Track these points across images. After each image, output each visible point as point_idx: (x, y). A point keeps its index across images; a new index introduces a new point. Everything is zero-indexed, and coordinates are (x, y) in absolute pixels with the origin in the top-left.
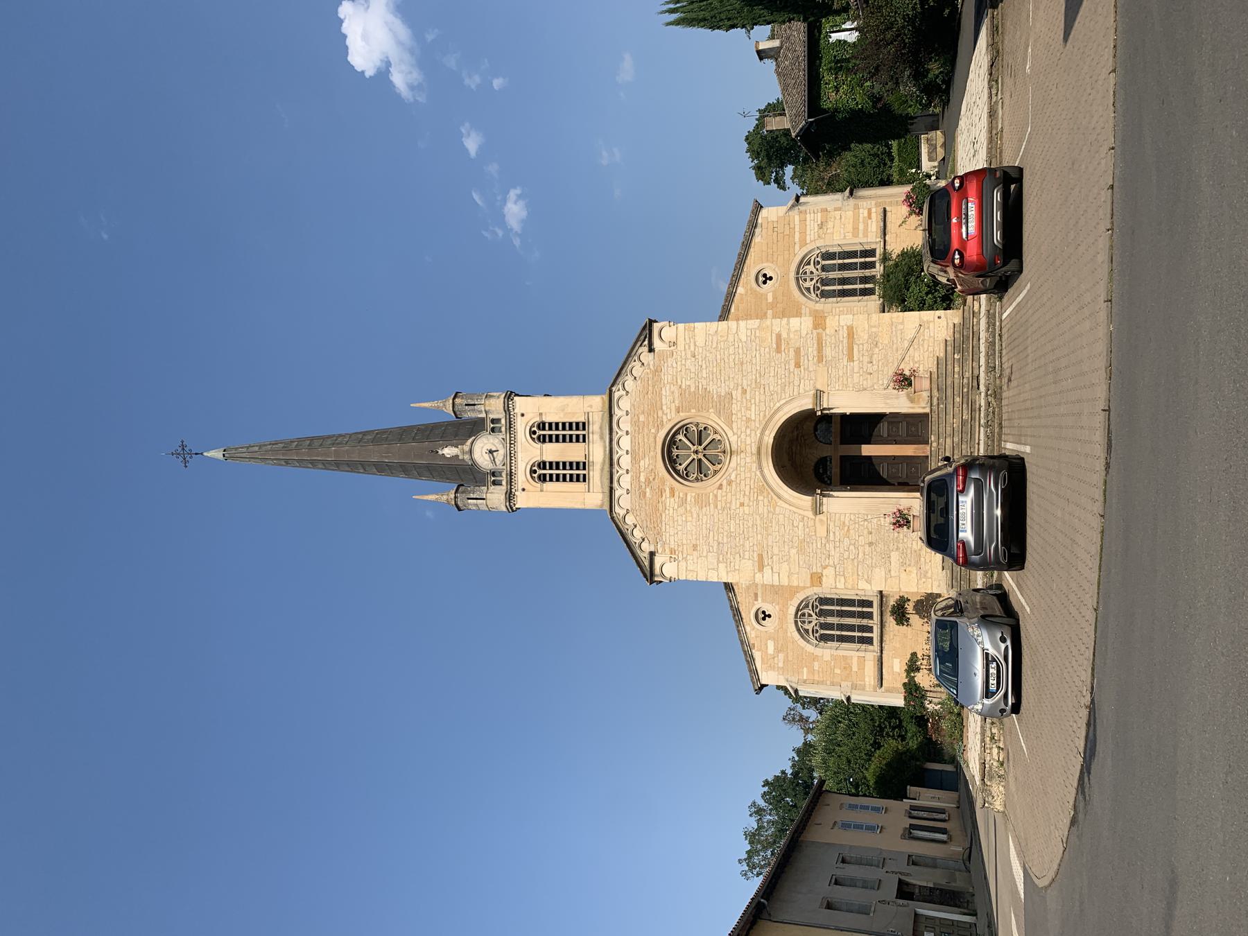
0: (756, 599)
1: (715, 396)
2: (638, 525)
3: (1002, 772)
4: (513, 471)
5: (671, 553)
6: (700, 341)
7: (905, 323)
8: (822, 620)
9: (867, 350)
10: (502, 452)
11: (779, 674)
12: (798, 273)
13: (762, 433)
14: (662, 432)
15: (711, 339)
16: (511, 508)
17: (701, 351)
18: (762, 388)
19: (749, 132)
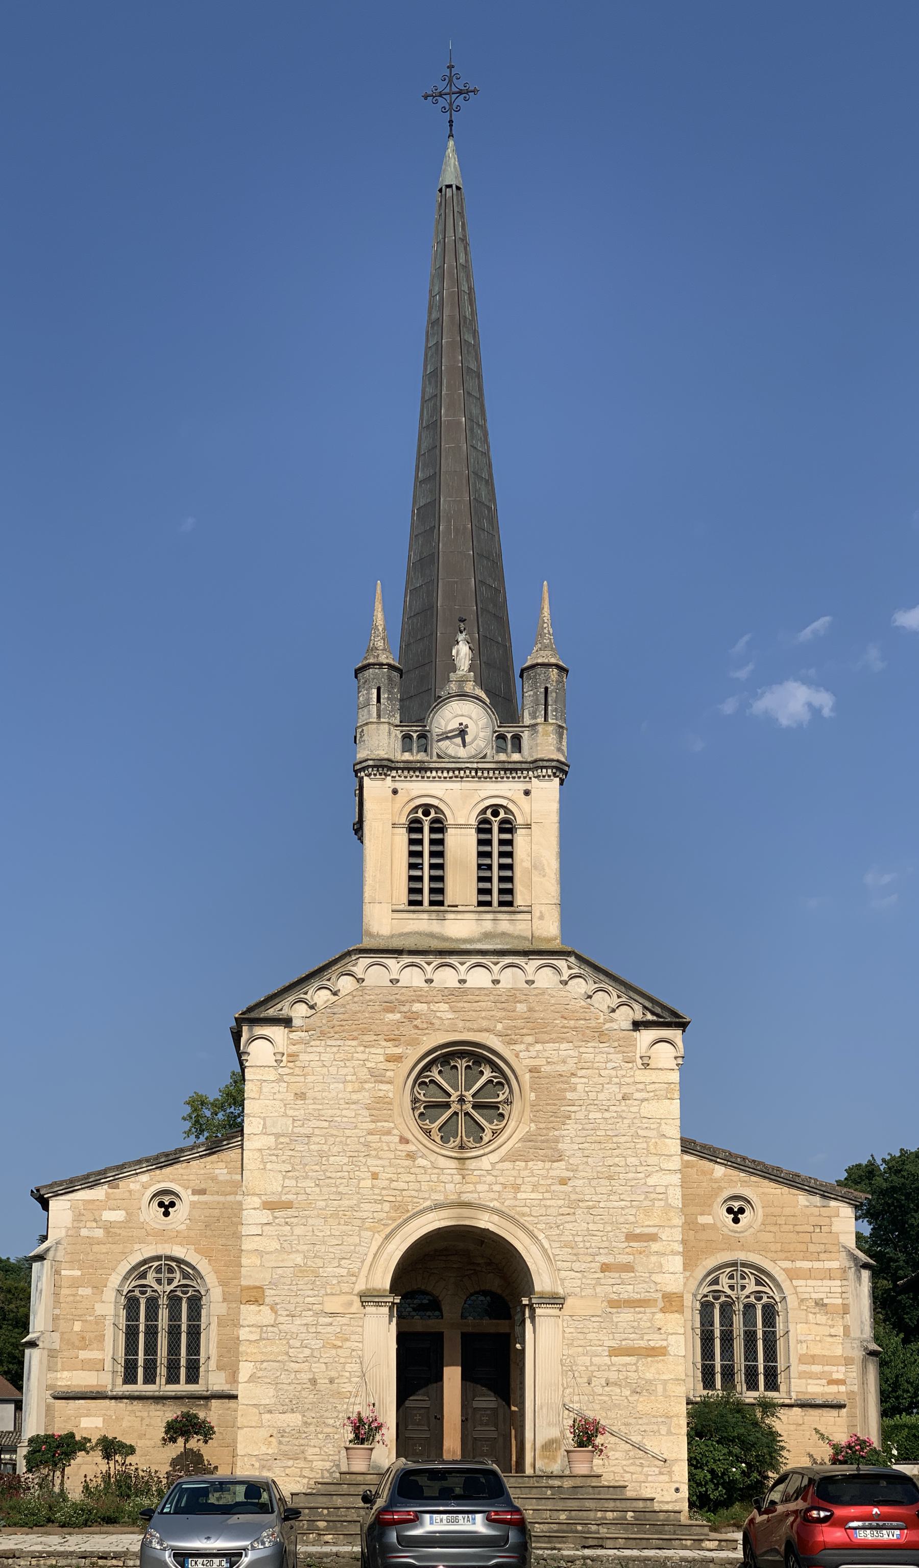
0: (195, 1192)
1: (556, 1133)
2: (337, 998)
4: (428, 774)
5: (289, 1055)
8: (163, 1301)
9: (627, 1378)
10: (462, 753)
11: (69, 1229)
12: (744, 1265)
13: (495, 1211)
15: (652, 1126)
16: (363, 769)
17: (633, 1109)
18: (568, 1210)
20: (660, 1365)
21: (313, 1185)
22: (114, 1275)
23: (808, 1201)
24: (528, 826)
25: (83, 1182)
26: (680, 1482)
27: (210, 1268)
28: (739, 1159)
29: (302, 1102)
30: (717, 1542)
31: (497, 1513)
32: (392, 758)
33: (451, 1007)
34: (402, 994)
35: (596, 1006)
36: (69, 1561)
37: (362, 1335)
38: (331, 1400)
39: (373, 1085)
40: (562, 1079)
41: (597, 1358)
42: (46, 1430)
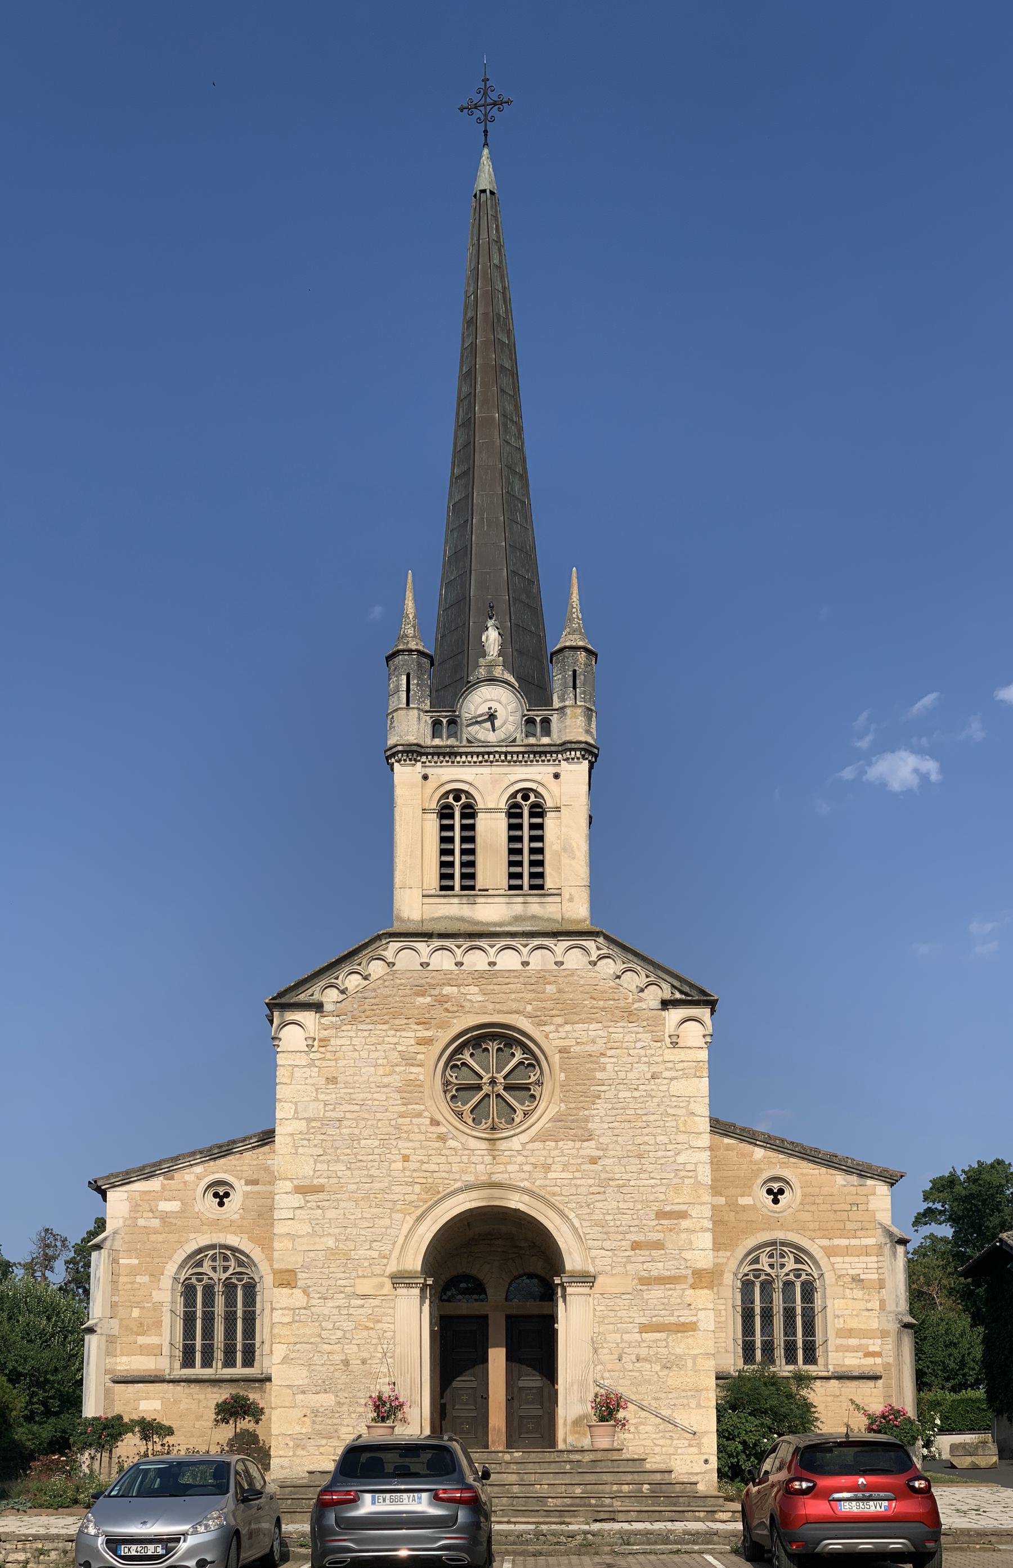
0: (247, 1183)
1: (586, 1113)
2: (367, 982)
4: (458, 759)
5: (321, 1040)
6: (678, 1087)
7: (701, 1411)
8: (219, 1288)
9: (657, 1354)
10: (492, 737)
11: (126, 1219)
12: (783, 1244)
14: (527, 1024)
15: (681, 1104)
18: (599, 1189)
20: (690, 1340)
21: (344, 1168)
22: (170, 1263)
23: (845, 1180)
24: (557, 809)
25: (139, 1173)
26: (710, 1454)
27: (263, 1256)
28: (778, 1142)
29: (334, 1086)
30: (731, 1513)
31: (445, 1491)
32: (422, 743)
33: (481, 990)
34: (432, 977)
35: (625, 986)
36: (55, 1545)
37: (394, 1316)
38: (363, 1380)
39: (404, 1068)
40: (591, 1059)
41: (627, 1335)
42: (105, 1413)
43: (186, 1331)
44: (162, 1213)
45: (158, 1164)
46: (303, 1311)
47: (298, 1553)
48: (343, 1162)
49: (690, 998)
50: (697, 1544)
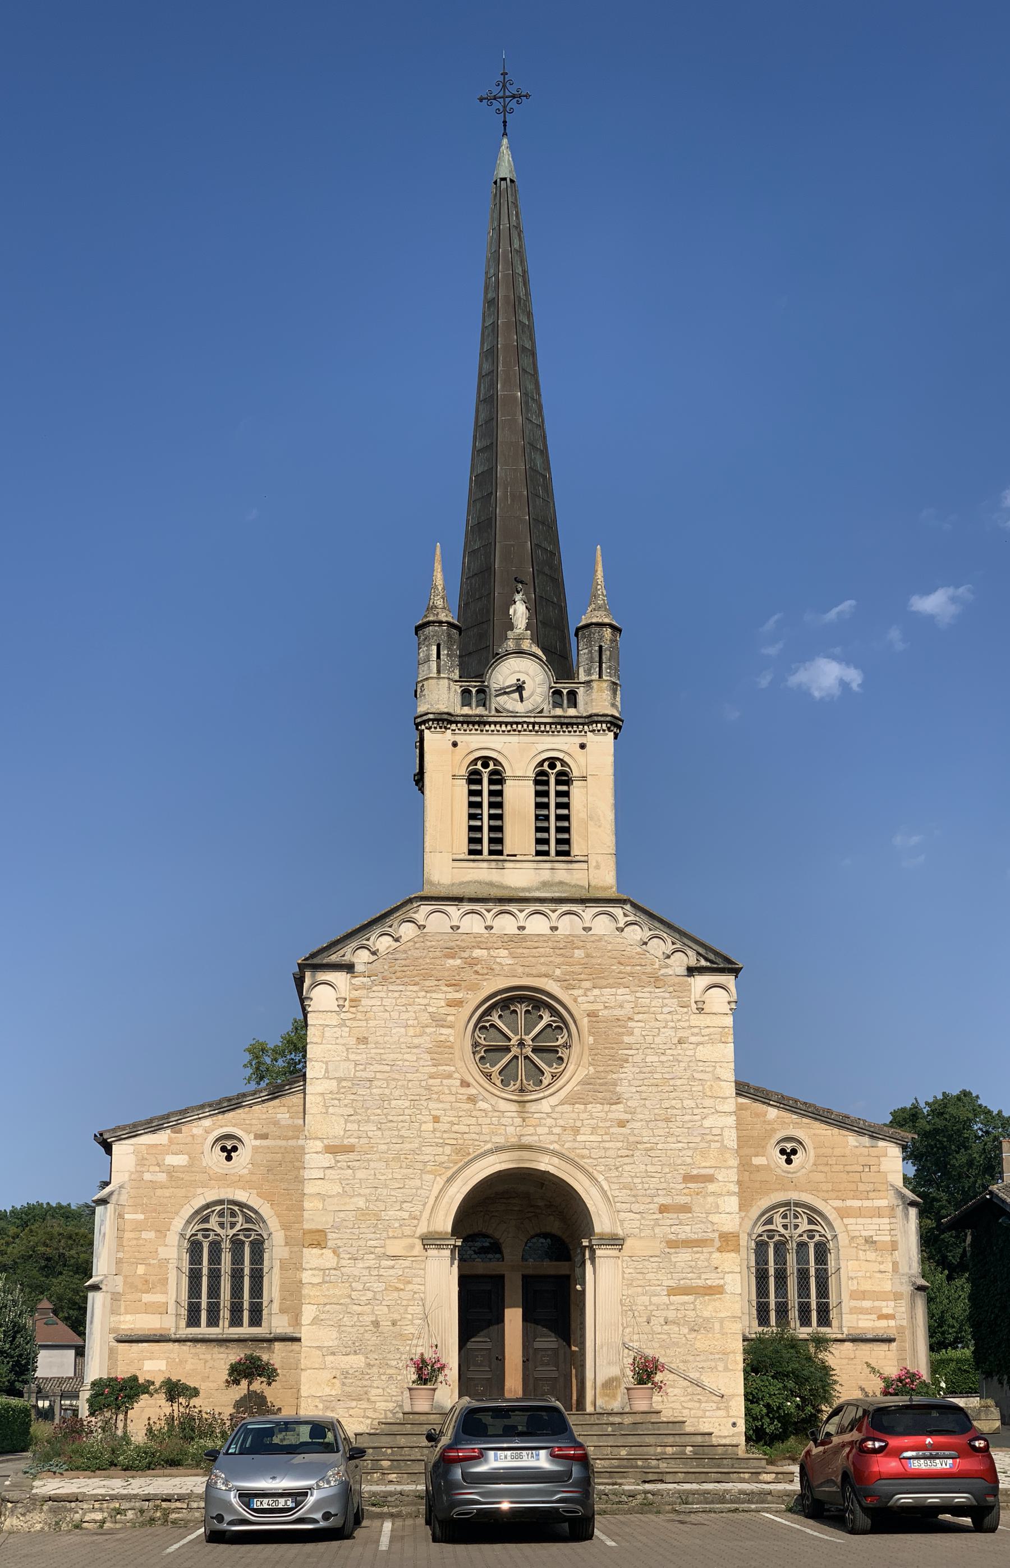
0: (257, 1137)
1: (614, 1076)
2: (398, 944)
3: (64, 1526)
4: (487, 727)
5: (351, 1000)
6: (703, 1052)
7: (728, 1374)
8: (226, 1245)
10: (520, 708)
11: (132, 1173)
12: (796, 1205)
13: (554, 1153)
14: (556, 988)
15: (708, 1069)
19: (977, 1097)
21: (375, 1128)
23: (857, 1141)
24: (584, 778)
25: (144, 1127)
27: (272, 1213)
28: (791, 1102)
29: (364, 1046)
30: (774, 1475)
31: (560, 1449)
32: (451, 711)
33: (510, 953)
34: (462, 940)
35: (652, 952)
36: (133, 1504)
37: (424, 1278)
38: (394, 1342)
40: (619, 1023)
42: (109, 1373)
43: (191, 1289)
44: (169, 1167)
45: (167, 1117)
46: (333, 1272)
47: (371, 1511)
48: (373, 1122)
49: (715, 966)
50: (753, 1503)
